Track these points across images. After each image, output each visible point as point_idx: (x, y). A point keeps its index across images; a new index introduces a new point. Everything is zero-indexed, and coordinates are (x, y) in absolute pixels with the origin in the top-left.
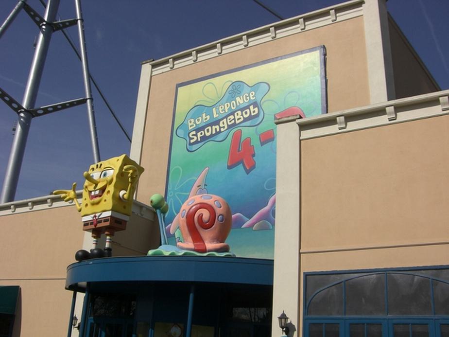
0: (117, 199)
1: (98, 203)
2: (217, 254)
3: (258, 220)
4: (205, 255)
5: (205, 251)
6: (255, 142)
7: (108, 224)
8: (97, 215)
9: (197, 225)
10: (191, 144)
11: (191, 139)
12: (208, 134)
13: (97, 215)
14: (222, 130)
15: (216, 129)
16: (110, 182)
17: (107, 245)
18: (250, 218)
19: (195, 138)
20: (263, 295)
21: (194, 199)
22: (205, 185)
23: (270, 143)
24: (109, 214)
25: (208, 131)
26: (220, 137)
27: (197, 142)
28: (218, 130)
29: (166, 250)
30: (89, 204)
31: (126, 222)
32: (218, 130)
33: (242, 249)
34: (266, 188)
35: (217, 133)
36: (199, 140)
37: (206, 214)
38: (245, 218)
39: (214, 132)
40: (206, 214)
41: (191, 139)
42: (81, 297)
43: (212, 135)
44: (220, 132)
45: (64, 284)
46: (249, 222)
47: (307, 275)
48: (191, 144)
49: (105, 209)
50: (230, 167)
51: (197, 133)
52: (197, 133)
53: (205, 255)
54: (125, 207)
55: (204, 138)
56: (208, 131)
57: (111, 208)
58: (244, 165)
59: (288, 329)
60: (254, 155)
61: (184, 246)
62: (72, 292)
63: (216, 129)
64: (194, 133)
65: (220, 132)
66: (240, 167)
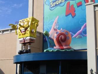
0: (31, 32)
1: (25, 34)
2: (67, 50)
3: (78, 35)
4: (63, 51)
5: (63, 49)
6: (75, 6)
7: (29, 41)
8: (25, 38)
9: (60, 40)
10: (51, 7)
11: (51, 5)
12: (57, 4)
13: (25, 38)
14: (63, 2)
15: (60, 2)
16: (29, 26)
17: (29, 49)
18: (75, 34)
19: (53, 5)
20: (85, 63)
21: (54, 26)
22: (58, 22)
23: (81, 6)
24: (29, 38)
25: (57, 2)
26: (62, 5)
27: (53, 7)
28: (61, 2)
29: (50, 49)
30: (21, 35)
31: (34, 40)
32: (61, 2)
33: (75, 46)
34: (80, 23)
35: (61, 3)
36: (54, 6)
37: (63, 37)
38: (73, 34)
39: (60, 3)
40: (63, 37)
41: (51, 5)
42: (18, 65)
43: (59, 4)
44: (62, 3)
45: (13, 61)
46: (75, 36)
47: (77, 4)
48: (51, 7)
49: (28, 37)
50: (66, 16)
51: (53, 3)
52: (53, 3)
53: (63, 51)
54: (34, 35)
55: (56, 5)
56: (57, 2)
57: (29, 36)
58: (71, 15)
59: (92, 73)
60: (75, 11)
61: (57, 47)
62: (16, 64)
63: (60, 2)
64: (52, 3)
65: (62, 3)
66: (70, 16)
